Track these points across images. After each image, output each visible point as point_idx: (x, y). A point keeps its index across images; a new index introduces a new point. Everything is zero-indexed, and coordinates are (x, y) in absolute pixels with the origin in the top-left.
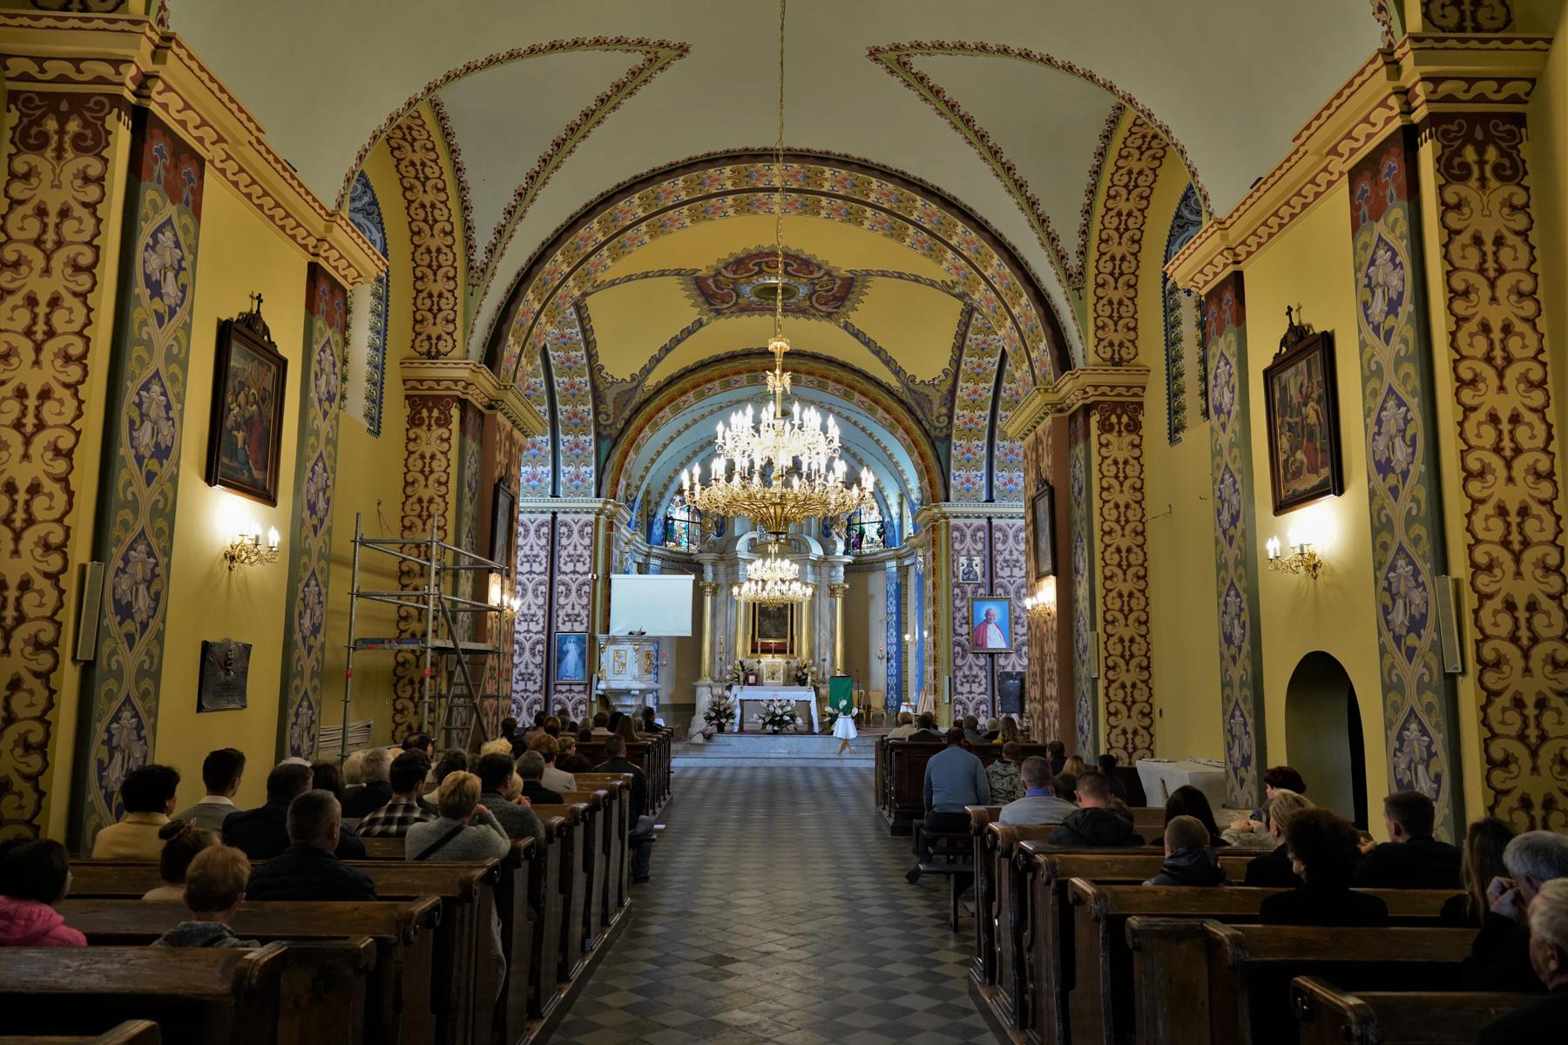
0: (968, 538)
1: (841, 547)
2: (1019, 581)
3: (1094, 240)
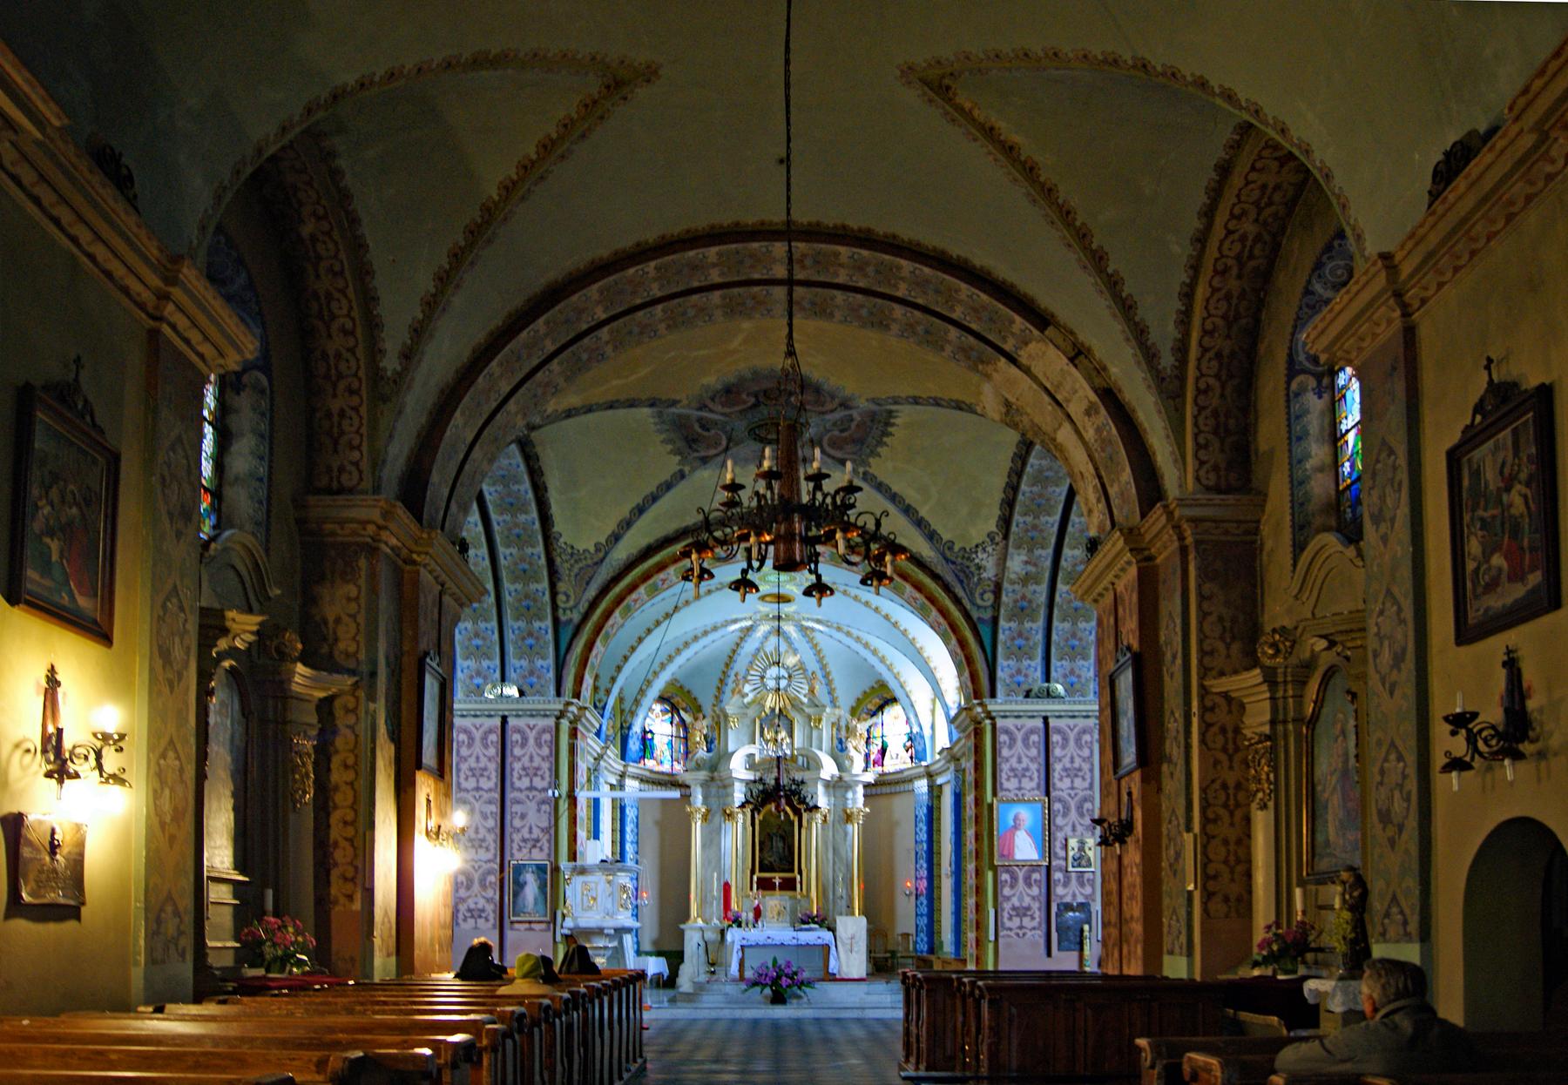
0: (1019, 743)
1: (859, 763)
2: (1081, 794)
3: (1195, 336)
